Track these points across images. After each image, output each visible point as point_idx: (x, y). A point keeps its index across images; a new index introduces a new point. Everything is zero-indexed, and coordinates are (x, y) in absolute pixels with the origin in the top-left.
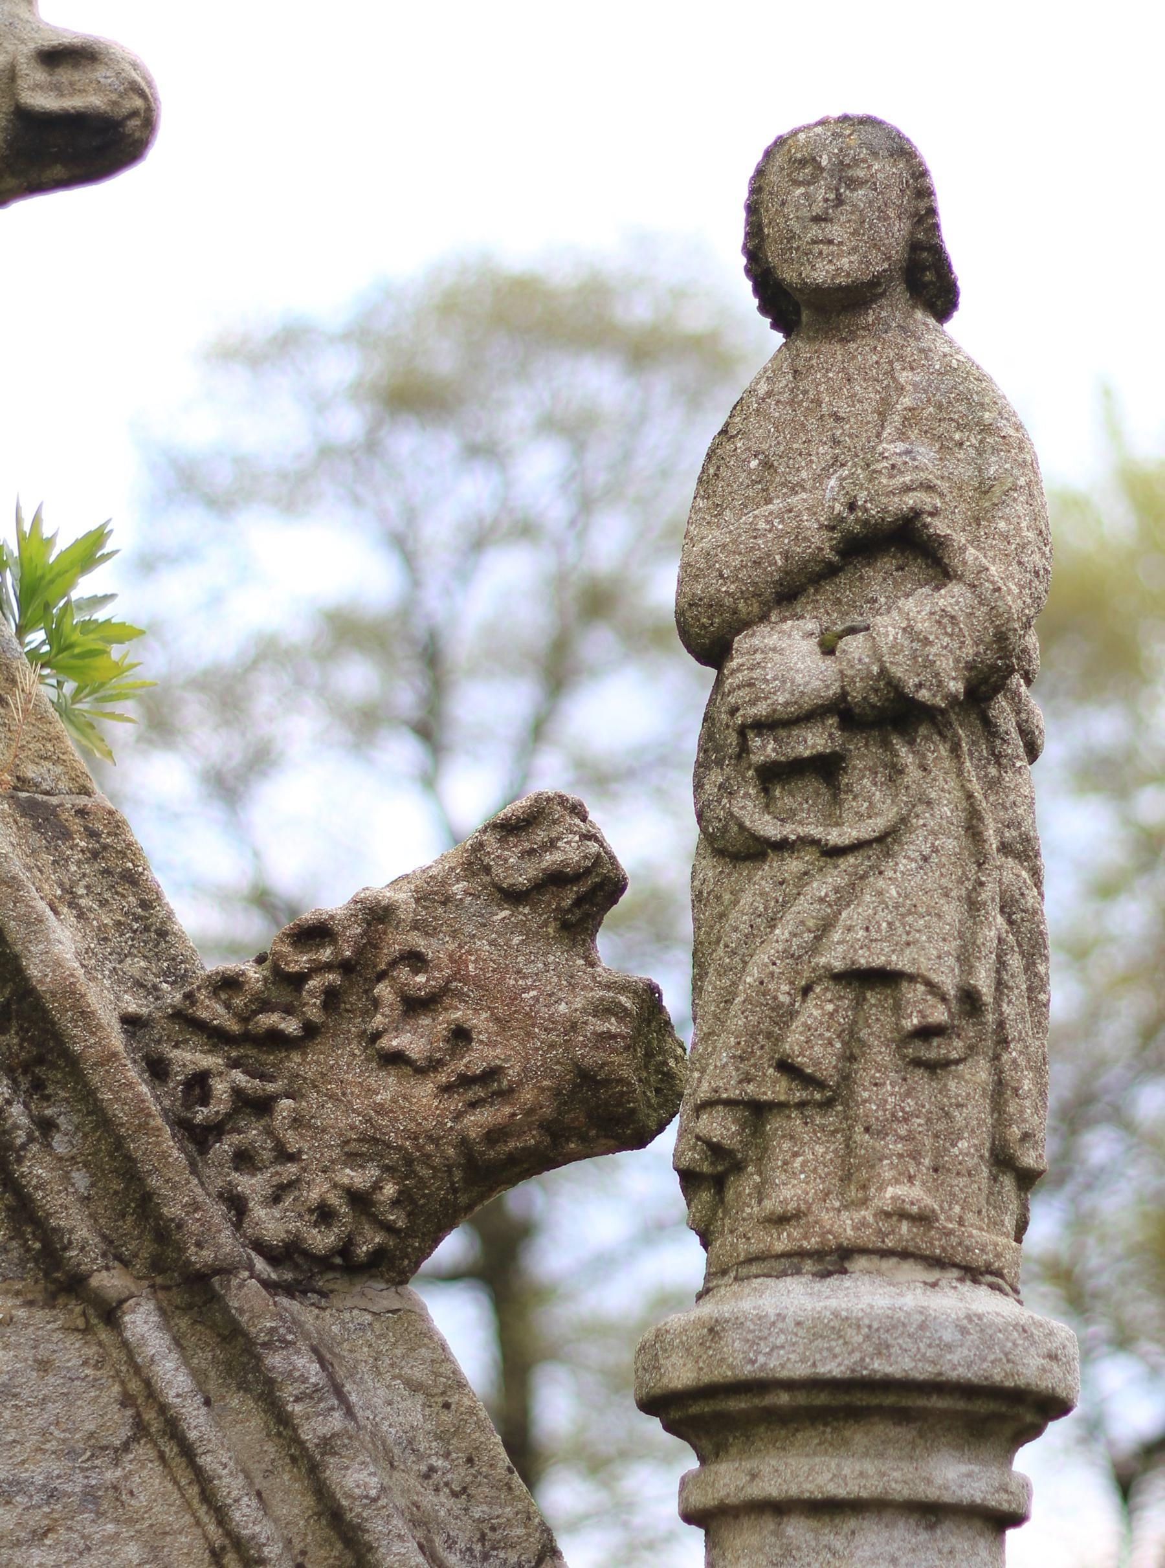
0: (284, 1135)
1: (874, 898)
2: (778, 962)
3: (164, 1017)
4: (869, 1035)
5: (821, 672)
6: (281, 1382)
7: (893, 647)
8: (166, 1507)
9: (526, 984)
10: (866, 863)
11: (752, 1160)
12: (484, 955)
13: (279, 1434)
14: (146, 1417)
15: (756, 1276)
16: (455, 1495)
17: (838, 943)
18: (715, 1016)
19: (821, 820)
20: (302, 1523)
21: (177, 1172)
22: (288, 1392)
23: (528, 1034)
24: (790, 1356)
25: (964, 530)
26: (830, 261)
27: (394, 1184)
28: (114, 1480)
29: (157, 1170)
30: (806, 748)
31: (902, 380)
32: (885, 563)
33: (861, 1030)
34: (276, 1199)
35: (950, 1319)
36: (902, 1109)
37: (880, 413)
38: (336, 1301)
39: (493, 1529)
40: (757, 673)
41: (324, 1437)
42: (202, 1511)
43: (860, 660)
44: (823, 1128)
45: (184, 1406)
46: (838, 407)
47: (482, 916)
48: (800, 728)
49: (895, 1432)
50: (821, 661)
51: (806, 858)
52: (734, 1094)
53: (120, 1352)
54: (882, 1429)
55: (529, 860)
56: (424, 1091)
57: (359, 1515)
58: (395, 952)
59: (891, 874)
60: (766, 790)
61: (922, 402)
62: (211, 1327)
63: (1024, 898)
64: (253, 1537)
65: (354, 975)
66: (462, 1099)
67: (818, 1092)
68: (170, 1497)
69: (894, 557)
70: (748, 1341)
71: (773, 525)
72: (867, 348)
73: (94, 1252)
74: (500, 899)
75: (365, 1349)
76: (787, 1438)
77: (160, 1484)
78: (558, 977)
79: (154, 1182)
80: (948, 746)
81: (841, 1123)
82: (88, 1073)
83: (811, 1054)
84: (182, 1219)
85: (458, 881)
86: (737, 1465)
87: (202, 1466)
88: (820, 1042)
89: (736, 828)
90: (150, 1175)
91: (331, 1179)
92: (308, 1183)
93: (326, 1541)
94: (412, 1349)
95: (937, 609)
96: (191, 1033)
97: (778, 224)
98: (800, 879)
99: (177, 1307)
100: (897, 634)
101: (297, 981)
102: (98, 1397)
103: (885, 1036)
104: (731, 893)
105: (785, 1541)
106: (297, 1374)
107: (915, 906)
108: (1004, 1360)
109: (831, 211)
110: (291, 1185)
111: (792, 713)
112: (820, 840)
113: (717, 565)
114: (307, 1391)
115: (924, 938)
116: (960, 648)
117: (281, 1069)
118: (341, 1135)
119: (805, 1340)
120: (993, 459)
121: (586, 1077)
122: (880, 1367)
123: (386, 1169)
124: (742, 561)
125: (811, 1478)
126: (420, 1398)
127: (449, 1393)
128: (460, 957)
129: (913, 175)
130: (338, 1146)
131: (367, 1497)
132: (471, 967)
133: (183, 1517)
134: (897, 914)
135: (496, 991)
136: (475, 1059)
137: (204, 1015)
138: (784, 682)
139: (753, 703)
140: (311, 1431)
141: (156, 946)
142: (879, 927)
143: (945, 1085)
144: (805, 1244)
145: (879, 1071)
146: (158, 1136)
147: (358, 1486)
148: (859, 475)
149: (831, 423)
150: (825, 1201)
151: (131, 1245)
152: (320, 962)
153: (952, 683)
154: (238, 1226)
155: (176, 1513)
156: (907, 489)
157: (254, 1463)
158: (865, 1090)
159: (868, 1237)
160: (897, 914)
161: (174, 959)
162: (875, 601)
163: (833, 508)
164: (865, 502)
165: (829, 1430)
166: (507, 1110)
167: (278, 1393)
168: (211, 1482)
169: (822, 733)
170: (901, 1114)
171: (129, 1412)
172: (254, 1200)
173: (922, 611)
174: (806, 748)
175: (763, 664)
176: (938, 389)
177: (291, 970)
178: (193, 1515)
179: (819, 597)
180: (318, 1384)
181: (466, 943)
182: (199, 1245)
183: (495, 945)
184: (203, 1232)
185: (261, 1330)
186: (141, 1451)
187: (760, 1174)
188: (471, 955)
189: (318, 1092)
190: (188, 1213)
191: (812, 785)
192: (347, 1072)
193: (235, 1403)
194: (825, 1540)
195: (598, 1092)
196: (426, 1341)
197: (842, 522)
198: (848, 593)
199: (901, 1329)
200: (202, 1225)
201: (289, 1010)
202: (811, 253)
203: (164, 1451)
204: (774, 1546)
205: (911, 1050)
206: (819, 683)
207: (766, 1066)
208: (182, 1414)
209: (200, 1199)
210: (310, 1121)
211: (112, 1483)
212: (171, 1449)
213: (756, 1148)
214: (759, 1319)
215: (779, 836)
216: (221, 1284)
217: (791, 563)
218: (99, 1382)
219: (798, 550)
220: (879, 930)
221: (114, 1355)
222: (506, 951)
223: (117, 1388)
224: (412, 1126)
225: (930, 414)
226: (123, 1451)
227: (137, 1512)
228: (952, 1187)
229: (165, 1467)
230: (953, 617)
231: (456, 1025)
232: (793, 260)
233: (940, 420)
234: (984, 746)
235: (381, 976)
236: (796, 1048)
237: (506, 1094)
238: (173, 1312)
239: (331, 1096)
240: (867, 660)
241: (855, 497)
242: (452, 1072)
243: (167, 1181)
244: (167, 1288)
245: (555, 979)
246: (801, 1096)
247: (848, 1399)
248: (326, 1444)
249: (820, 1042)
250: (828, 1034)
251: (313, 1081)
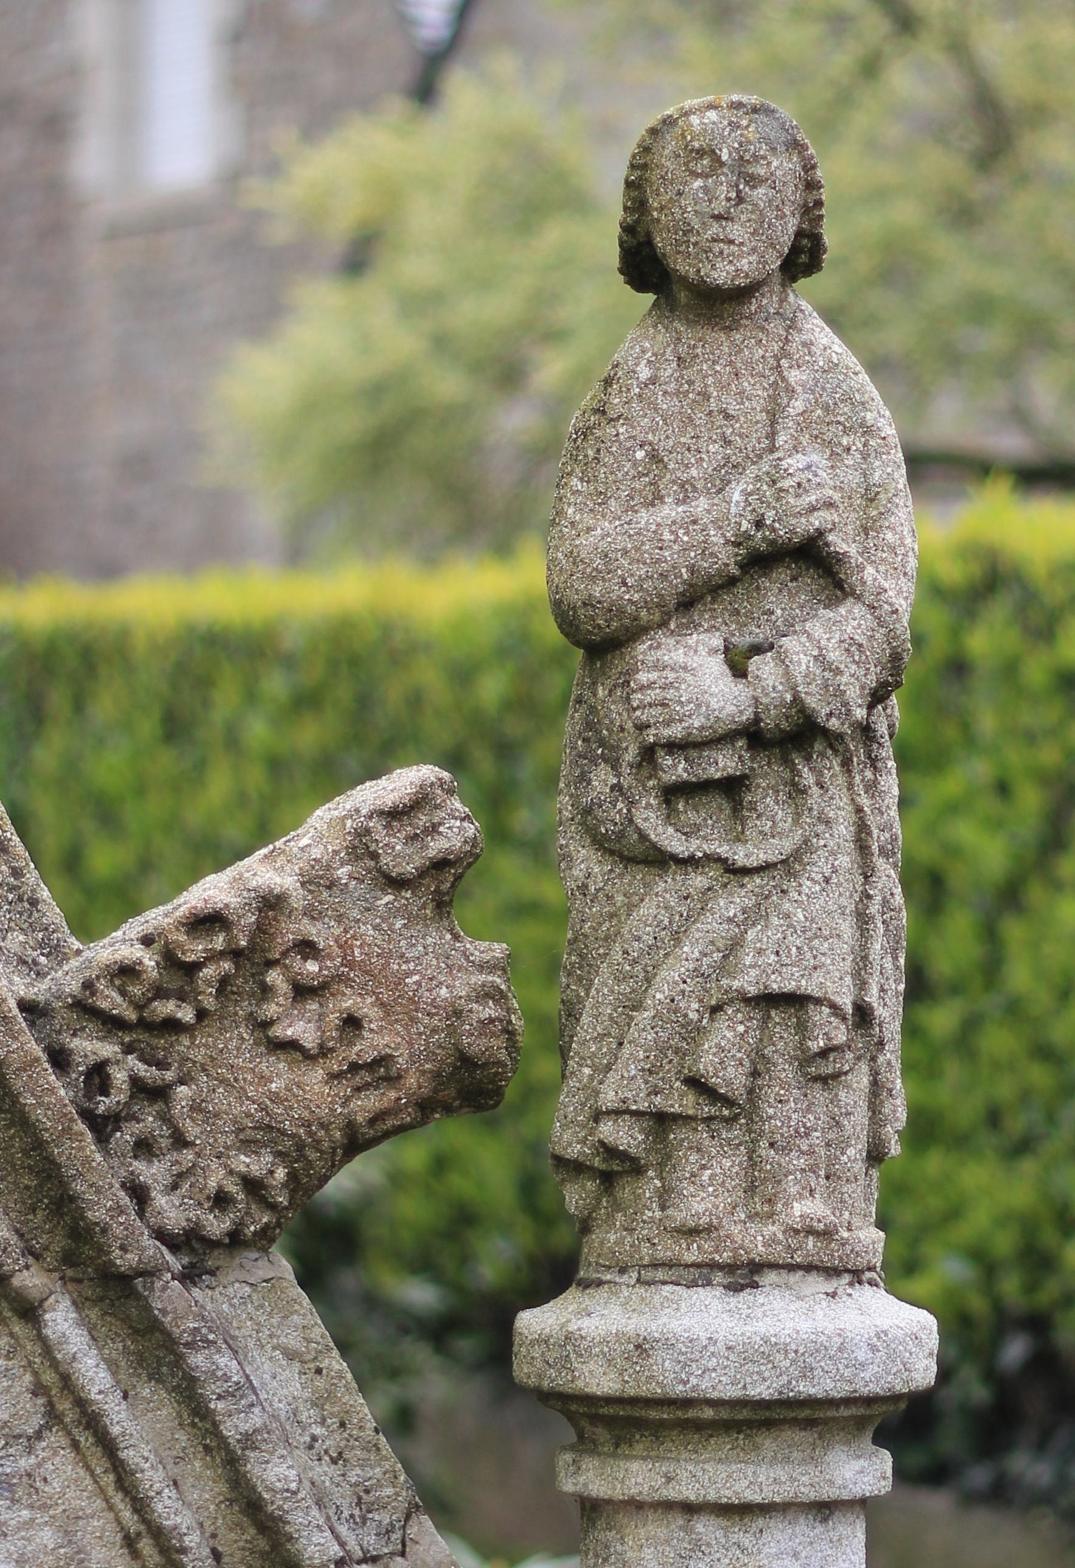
0: (183, 1125)
1: (782, 921)
2: (689, 980)
3: (65, 1007)
4: (773, 1052)
5: (735, 697)
6: (204, 1381)
7: (806, 676)
8: (78, 1493)
9: (409, 969)
10: (771, 883)
11: (652, 1165)
12: (369, 940)
13: (193, 1425)
14: (60, 1407)
15: (664, 1283)
16: (334, 1461)
17: (751, 966)
18: (611, 1018)
19: (724, 836)
20: (212, 1507)
21: (100, 1176)
22: (210, 1390)
23: (412, 1019)
24: (721, 1379)
25: (855, 541)
26: (731, 262)
27: (284, 1167)
28: (27, 1468)
29: (81, 1175)
30: (717, 770)
31: (792, 380)
32: (780, 574)
33: (766, 1047)
35: (864, 1340)
36: (804, 1126)
37: (768, 412)
38: (221, 1277)
39: (367, 1491)
40: (671, 694)
41: (247, 1433)
42: (117, 1499)
43: (774, 688)
44: (729, 1142)
45: (106, 1403)
46: (727, 404)
47: (366, 900)
48: (711, 749)
49: (799, 1436)
50: (733, 685)
51: (711, 874)
52: (643, 1106)
53: (35, 1344)
54: (790, 1435)
55: (412, 845)
57: (280, 1508)
58: (289, 941)
59: (794, 895)
60: (667, 802)
61: (810, 403)
62: (122, 1320)
63: (893, 897)
64: (175, 1527)
65: (242, 959)
66: (350, 1084)
67: (726, 1109)
68: (82, 1483)
69: (789, 567)
70: (680, 1362)
71: (678, 537)
72: (753, 341)
73: (15, 1252)
74: (385, 884)
75: (249, 1323)
76: (700, 1442)
77: (72, 1470)
78: (437, 959)
79: (78, 1187)
80: (839, 760)
81: (744, 1135)
82: (11, 1078)
83: (724, 1075)
84: (107, 1223)
85: (342, 865)
86: (650, 1466)
87: (124, 1460)
88: (733, 1063)
89: (635, 836)
90: (74, 1180)
91: (226, 1166)
92: (202, 1169)
93: (237, 1525)
94: (285, 1317)
95: (846, 637)
96: (87, 1020)
97: (673, 214)
98: (704, 894)
99: (87, 1299)
100: (809, 661)
101: (192, 969)
102: (11, 1386)
103: (789, 1053)
104: (625, 895)
105: (694, 1536)
106: (220, 1373)
107: (820, 929)
109: (732, 210)
110: (190, 1171)
111: (706, 737)
112: (727, 859)
113: (620, 572)
114: (230, 1389)
115: (829, 961)
116: (866, 675)
117: (171, 1053)
118: (236, 1122)
119: (736, 1364)
120: (877, 463)
121: (465, 1061)
122: (805, 1389)
123: (278, 1154)
124: (648, 572)
125: (728, 1485)
126: (297, 1366)
127: (320, 1358)
128: (346, 942)
129: (804, 167)
130: (233, 1132)
131: (287, 1490)
132: (357, 952)
133: (95, 1502)
134: (805, 939)
135: (381, 976)
136: (367, 1047)
137: (104, 1005)
138: (699, 706)
139: (668, 723)
140: (231, 1429)
141: (30, 917)
142: (789, 952)
143: (836, 1095)
144: (717, 1258)
145: (783, 1088)
146: (80, 1141)
147: (279, 1481)
148: (765, 492)
149: (720, 420)
150: (733, 1214)
151: (42, 1238)
152: (215, 951)
153: (859, 710)
154: (141, 1213)
155: (89, 1498)
156: (813, 509)
157: (165, 1449)
158: (770, 1107)
159: (779, 1254)
160: (805, 939)
161: (46, 929)
162: (772, 613)
163: (740, 525)
164: (773, 521)
165: (741, 1436)
166: (393, 1095)
167: (200, 1391)
168: (133, 1475)
169: (732, 755)
170: (803, 1130)
171: (41, 1401)
172: (155, 1189)
173: (831, 638)
174: (717, 770)
175: (677, 685)
176: (824, 389)
177: (187, 960)
178: (107, 1501)
179: (716, 606)
180: (240, 1383)
181: (351, 928)
182: (123, 1248)
183: (379, 930)
184: (127, 1237)
185: (184, 1331)
186: (53, 1439)
187: (662, 1179)
188: (356, 940)
189: (207, 1076)
190: (111, 1219)
191: (718, 802)
192: (237, 1057)
193: (146, 1392)
194: (734, 1537)
195: (475, 1073)
196: (297, 1307)
197: (749, 539)
198: (745, 604)
199: (823, 1352)
200: (126, 1229)
201: (182, 997)
202: (711, 251)
203: (79, 1441)
204: (683, 1540)
205: (814, 1069)
206: (734, 708)
207: (673, 1079)
208: (105, 1410)
209: (122, 1203)
210: (200, 1104)
211: (26, 1471)
212: (87, 1440)
213: (656, 1153)
214: (691, 1342)
215: (686, 853)
216: (144, 1286)
217: (697, 577)
218: (12, 1372)
219: (705, 565)
220: (789, 956)
221: (29, 1347)
222: (389, 935)
223: (28, 1378)
224: (306, 1114)
225: (819, 417)
226: (36, 1439)
227: (51, 1499)
228: (842, 1194)
229: (78, 1453)
230: (860, 645)
231: (348, 1014)
232: (690, 255)
233: (828, 424)
234: (862, 750)
235: (270, 964)
236: (711, 1069)
237: (393, 1080)
238: (83, 1304)
239: (223, 1081)
240: (780, 688)
241: (763, 515)
242: (343, 1060)
243: (91, 1186)
244: (79, 1281)
245: (434, 962)
246: (710, 1112)
247: (767, 1414)
248: (248, 1440)
249: (733, 1063)
250: (739, 1055)
251: (202, 1065)
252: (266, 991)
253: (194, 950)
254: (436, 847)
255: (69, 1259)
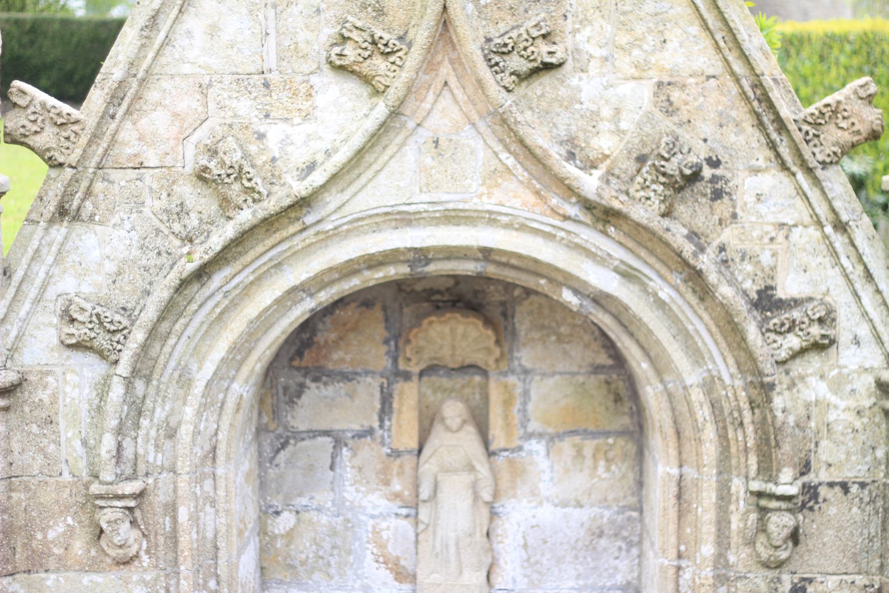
34: (820, 152)
56: (846, 134)
108: (503, 75)
121: (874, 131)
136: (855, 128)
140: (830, 196)
237: (860, 134)
252: (837, 118)
253: (825, 110)
254: (869, 92)
255: (801, 165)
